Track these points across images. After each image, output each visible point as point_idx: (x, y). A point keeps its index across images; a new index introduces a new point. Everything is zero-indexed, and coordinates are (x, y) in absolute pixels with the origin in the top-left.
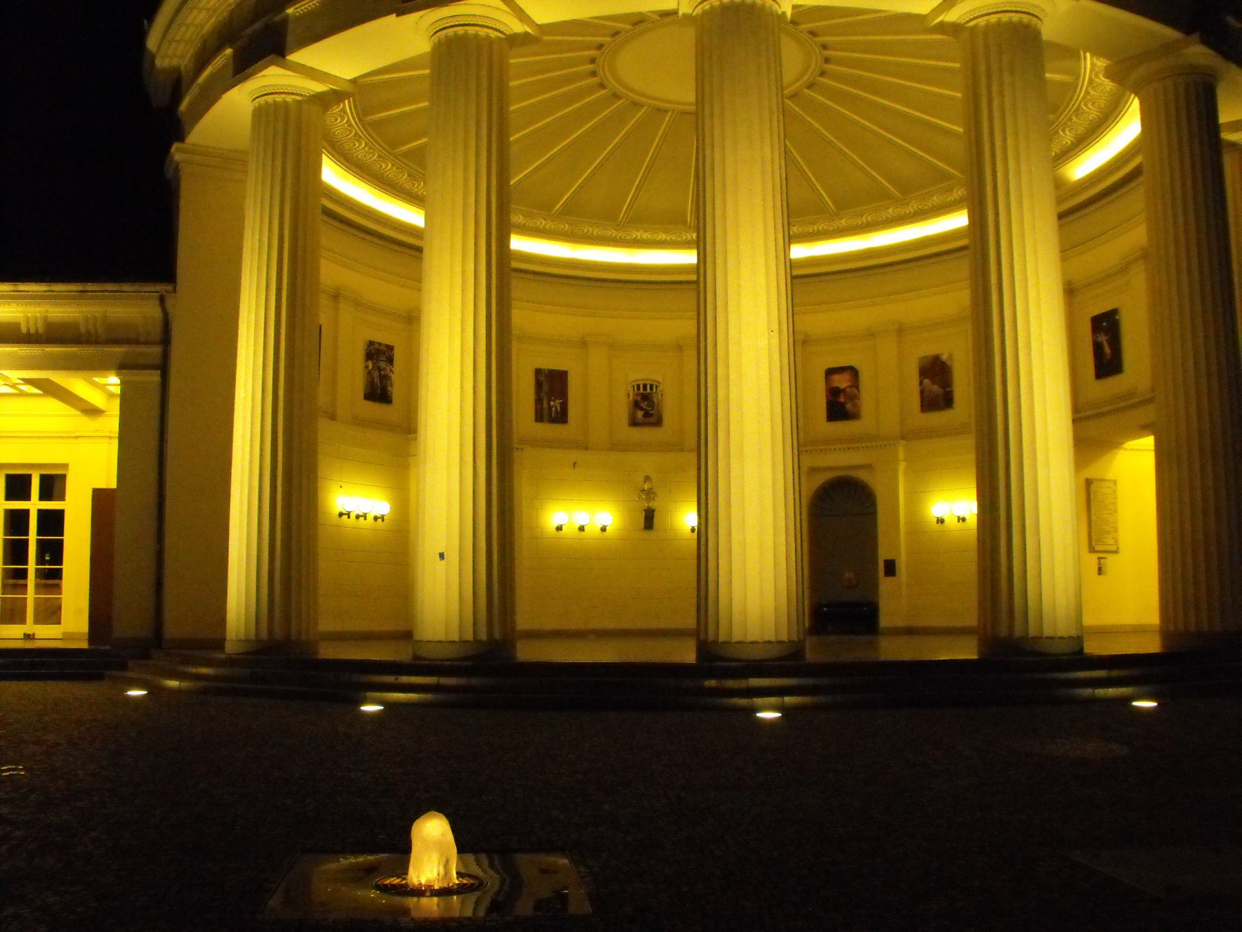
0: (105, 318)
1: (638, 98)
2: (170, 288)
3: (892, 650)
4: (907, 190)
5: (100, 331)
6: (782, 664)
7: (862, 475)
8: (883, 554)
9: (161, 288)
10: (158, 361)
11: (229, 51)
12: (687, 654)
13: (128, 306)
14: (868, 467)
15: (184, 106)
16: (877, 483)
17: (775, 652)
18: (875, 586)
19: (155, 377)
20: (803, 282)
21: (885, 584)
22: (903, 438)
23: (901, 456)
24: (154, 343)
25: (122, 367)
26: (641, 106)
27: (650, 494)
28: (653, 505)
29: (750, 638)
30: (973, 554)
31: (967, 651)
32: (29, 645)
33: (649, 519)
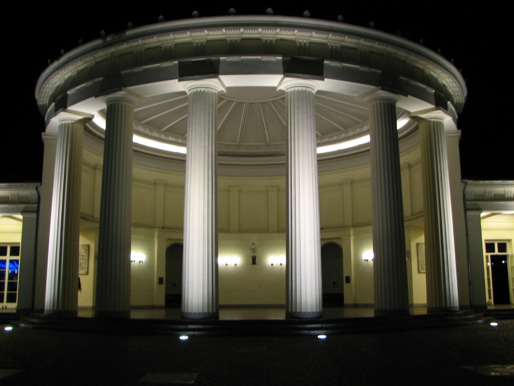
0: (18, 194)
1: (232, 99)
2: (39, 184)
3: (350, 313)
4: (346, 127)
5: (16, 199)
6: (319, 320)
7: (337, 241)
8: (345, 274)
9: (36, 184)
10: (36, 209)
11: (53, 104)
12: (280, 316)
13: (26, 191)
14: (339, 238)
15: (46, 119)
16: (343, 244)
17: (315, 316)
18: (342, 288)
19: (34, 215)
20: (324, 163)
21: (346, 285)
22: (353, 226)
23: (352, 233)
24: (35, 203)
25: (23, 212)
26: (233, 102)
27: (254, 250)
28: (255, 254)
29: (194, 312)
30: (372, 274)
31: (370, 314)
32: (4, 311)
33: (254, 260)
